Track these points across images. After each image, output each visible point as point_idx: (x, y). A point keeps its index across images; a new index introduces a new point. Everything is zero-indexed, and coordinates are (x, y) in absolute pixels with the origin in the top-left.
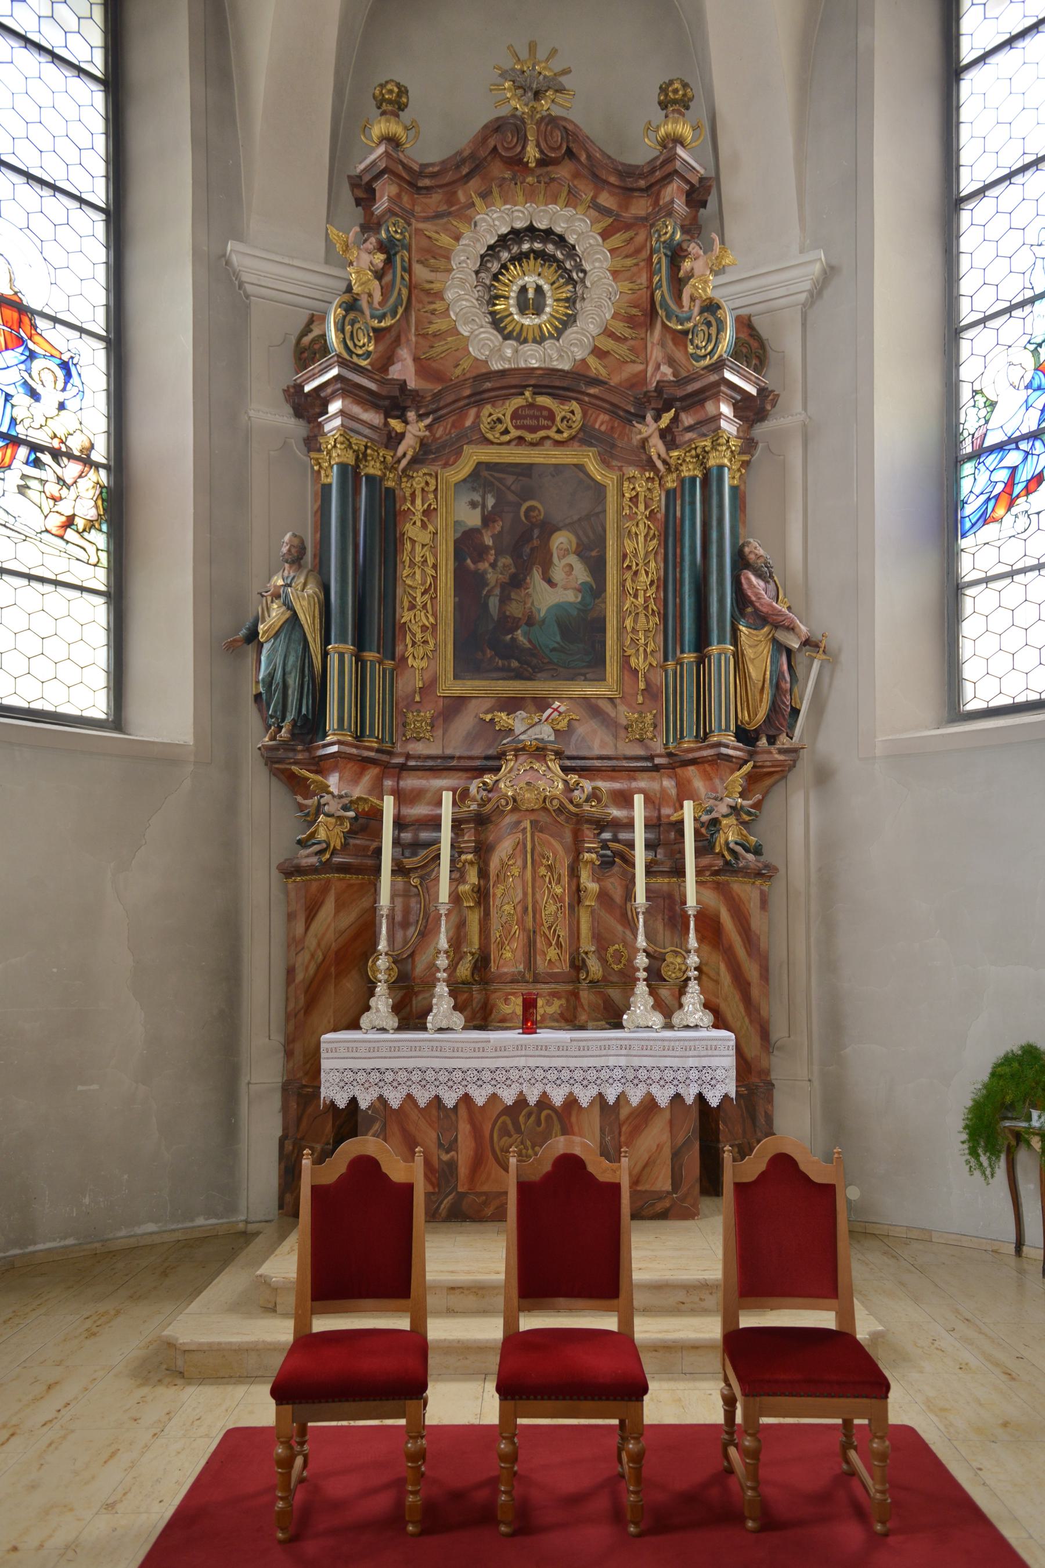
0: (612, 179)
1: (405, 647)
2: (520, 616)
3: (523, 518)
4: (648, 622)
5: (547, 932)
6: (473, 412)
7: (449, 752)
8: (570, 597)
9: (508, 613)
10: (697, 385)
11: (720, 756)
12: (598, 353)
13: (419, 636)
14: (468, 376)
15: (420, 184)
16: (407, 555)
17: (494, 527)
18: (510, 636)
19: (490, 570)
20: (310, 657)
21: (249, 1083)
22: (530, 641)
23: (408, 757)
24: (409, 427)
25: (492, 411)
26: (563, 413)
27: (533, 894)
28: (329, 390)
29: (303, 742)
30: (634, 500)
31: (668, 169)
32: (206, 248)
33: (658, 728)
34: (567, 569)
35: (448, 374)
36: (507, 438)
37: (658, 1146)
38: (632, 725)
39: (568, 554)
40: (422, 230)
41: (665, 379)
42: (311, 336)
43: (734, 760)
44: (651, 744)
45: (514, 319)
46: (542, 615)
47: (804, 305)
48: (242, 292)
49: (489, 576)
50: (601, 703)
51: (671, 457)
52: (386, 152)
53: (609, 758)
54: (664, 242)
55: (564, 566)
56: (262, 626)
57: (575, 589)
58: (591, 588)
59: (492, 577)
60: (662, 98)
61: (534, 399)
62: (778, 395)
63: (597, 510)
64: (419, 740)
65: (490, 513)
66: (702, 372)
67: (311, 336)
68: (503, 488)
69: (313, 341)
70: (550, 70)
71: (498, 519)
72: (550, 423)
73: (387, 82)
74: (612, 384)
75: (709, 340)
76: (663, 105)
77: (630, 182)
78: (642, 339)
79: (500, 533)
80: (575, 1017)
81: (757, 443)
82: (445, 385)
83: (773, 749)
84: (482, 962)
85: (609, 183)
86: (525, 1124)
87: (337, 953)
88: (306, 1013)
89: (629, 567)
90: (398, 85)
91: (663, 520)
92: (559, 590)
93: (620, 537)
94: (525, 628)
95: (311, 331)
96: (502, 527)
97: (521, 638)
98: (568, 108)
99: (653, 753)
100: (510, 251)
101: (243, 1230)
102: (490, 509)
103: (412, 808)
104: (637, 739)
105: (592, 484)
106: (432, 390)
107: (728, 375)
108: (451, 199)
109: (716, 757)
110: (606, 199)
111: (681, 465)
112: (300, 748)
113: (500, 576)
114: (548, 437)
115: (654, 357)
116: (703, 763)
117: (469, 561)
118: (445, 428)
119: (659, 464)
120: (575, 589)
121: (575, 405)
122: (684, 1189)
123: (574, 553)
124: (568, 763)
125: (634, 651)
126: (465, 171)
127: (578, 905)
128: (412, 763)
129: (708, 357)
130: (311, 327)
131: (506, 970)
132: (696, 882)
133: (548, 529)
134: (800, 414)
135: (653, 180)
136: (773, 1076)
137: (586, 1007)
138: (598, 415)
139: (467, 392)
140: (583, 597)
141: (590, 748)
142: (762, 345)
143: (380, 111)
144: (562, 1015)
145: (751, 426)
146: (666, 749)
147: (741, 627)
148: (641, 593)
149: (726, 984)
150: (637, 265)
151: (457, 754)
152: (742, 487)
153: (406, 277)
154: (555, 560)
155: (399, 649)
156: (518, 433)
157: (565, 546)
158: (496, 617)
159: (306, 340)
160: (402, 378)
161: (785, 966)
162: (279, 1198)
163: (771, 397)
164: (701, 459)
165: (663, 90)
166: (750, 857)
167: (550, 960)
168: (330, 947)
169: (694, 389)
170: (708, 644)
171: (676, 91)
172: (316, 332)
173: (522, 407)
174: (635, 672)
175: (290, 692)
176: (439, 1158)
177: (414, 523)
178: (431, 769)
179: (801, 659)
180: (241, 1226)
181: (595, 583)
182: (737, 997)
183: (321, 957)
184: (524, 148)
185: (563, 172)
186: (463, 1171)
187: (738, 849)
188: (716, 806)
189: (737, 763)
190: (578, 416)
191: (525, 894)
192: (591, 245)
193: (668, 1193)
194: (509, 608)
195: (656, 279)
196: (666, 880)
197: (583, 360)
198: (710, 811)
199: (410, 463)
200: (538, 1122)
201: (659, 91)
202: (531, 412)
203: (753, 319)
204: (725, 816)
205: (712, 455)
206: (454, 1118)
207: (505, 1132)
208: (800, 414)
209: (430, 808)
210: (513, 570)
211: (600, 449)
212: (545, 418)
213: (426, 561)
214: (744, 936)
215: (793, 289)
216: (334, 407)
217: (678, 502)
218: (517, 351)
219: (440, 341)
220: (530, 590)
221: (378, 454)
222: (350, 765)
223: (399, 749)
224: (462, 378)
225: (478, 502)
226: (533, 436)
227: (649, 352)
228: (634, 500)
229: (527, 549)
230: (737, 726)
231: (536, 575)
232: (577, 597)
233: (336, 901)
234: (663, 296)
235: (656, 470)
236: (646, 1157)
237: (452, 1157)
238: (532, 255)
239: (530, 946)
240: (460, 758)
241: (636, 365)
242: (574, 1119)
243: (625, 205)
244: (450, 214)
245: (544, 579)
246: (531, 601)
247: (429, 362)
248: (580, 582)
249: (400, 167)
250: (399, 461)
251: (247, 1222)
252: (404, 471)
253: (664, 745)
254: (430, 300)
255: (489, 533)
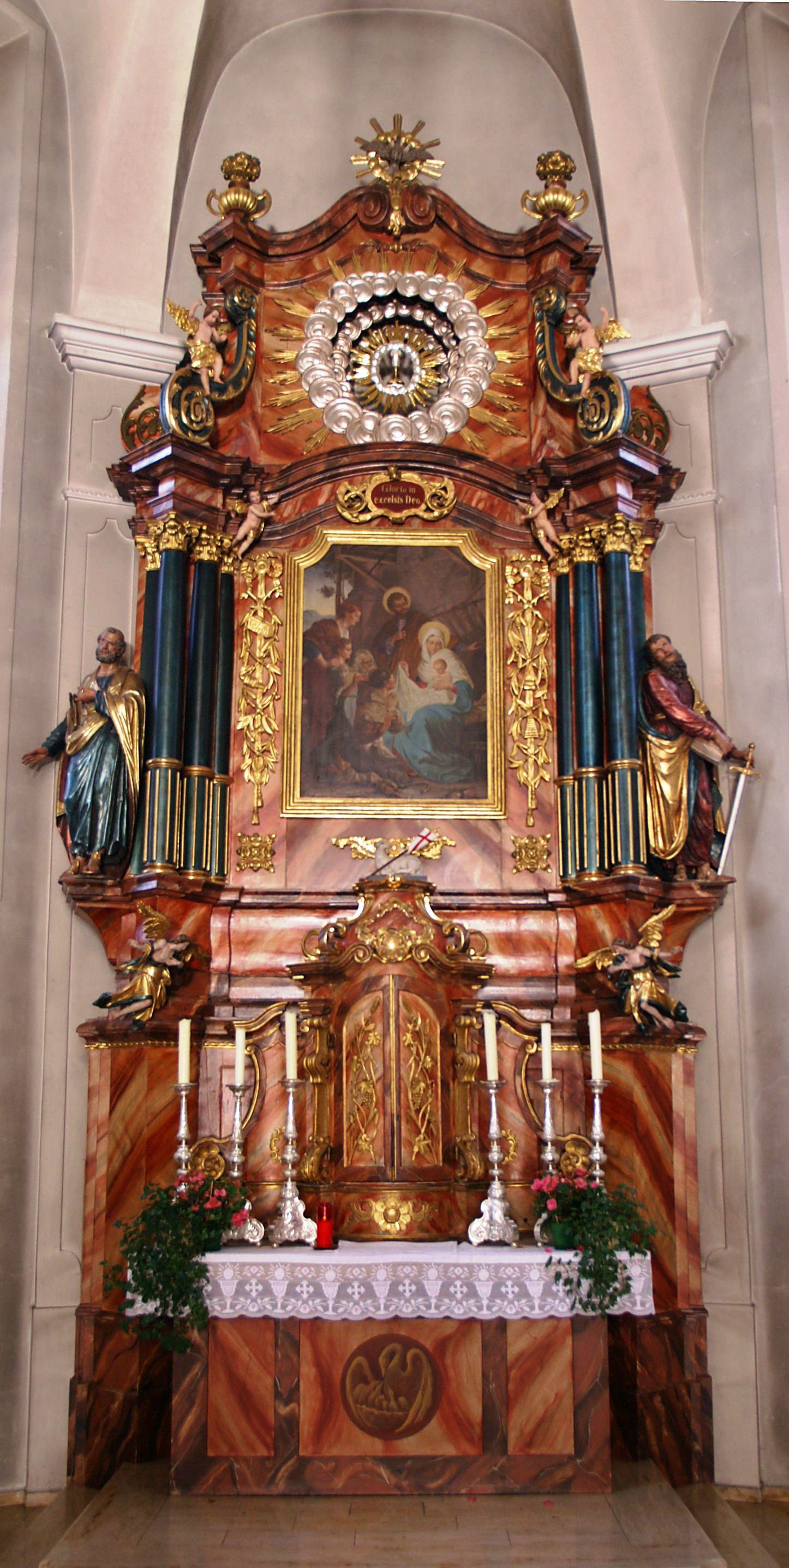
0: (487, 247)
1: (241, 760)
2: (382, 721)
3: (386, 607)
4: (539, 729)
5: (413, 1114)
6: (327, 489)
7: (293, 886)
8: (443, 698)
9: (367, 718)
10: (589, 464)
11: (628, 893)
12: (475, 425)
13: (258, 746)
14: (322, 450)
15: (271, 253)
16: (246, 650)
17: (351, 618)
18: (369, 745)
19: (346, 667)
20: (126, 772)
21: (34, 1307)
22: (394, 751)
23: (242, 892)
24: (252, 508)
25: (349, 487)
26: (434, 490)
27: (398, 1069)
28: (160, 470)
29: (114, 876)
30: (519, 586)
31: (550, 238)
32: (27, 321)
33: (553, 856)
34: (439, 666)
35: (300, 449)
36: (368, 517)
37: (557, 1395)
38: (520, 851)
39: (441, 648)
40: (272, 299)
41: (552, 455)
42: (141, 409)
43: (646, 898)
44: (545, 875)
45: (376, 389)
46: (409, 719)
47: (710, 376)
48: (65, 364)
49: (345, 674)
50: (481, 825)
51: (561, 540)
52: (234, 223)
53: (492, 894)
54: (548, 311)
55: (436, 663)
56: (69, 737)
57: (448, 689)
58: (468, 687)
59: (348, 675)
60: (542, 168)
61: (399, 475)
62: (684, 474)
63: (474, 598)
64: (256, 871)
65: (345, 601)
66: (594, 450)
67: (141, 409)
68: (363, 574)
69: (144, 414)
70: (418, 142)
71: (355, 607)
72: (418, 501)
73: (237, 155)
74: (491, 460)
75: (602, 416)
76: (542, 176)
77: (506, 250)
78: (525, 411)
79: (359, 623)
80: (451, 1226)
81: (662, 525)
82: (294, 461)
83: (693, 884)
84: (334, 1153)
85: (483, 251)
86: (387, 1366)
87: (149, 1141)
88: (107, 1218)
89: (514, 663)
90: (249, 158)
91: (554, 609)
92: (429, 690)
93: (501, 630)
94: (388, 735)
95: (142, 403)
96: (361, 618)
97: (383, 747)
98: (436, 178)
99: (547, 888)
100: (371, 317)
101: (21, 1501)
102: (346, 596)
103: (246, 956)
104: (527, 869)
105: (468, 567)
106: (279, 466)
107: (624, 454)
108: (305, 267)
109: (622, 895)
110: (479, 267)
111: (573, 549)
112: (110, 882)
113: (358, 674)
114: (416, 516)
115: (538, 431)
116: (608, 901)
117: (320, 657)
118: (295, 507)
119: (548, 547)
120: (448, 689)
121: (448, 482)
122: (590, 1452)
123: (448, 647)
124: (441, 900)
125: (521, 762)
126: (322, 239)
127: (454, 1081)
128: (246, 900)
129: (601, 434)
130: (142, 399)
131: (362, 1165)
132: (603, 1051)
133: (416, 619)
134: (711, 493)
135: (533, 249)
136: (707, 1300)
137: (464, 1213)
138: (476, 491)
139: (321, 468)
140: (458, 699)
141: (469, 881)
142: (665, 419)
143: (228, 182)
144: (433, 1223)
145: (655, 506)
146: (563, 882)
147: (650, 737)
148: (529, 694)
149: (642, 1183)
150: (517, 333)
151: (304, 889)
152: (646, 574)
153: (254, 346)
154: (425, 654)
155: (234, 761)
156: (380, 512)
157: (435, 639)
158: (352, 723)
159: (136, 413)
160: (246, 456)
161: (719, 1156)
162: (69, 1465)
163: (676, 476)
164: (598, 545)
165: (542, 161)
166: (668, 1022)
167: (418, 1153)
168: (140, 1134)
169: (587, 467)
170: (612, 757)
171: (556, 163)
172: (148, 404)
173: (386, 483)
174: (524, 787)
175: (101, 814)
176: (275, 1411)
177: (255, 614)
178: (271, 907)
179: (724, 773)
180: (19, 1498)
181: (474, 682)
182: (658, 1198)
183: (128, 1147)
184: (388, 217)
185: (433, 238)
186: (306, 1428)
187: (653, 1011)
188: (626, 955)
189: (649, 902)
190: (450, 495)
191: (386, 1068)
192: (464, 313)
193: (570, 1458)
194: (368, 711)
195: (539, 349)
196: (565, 1048)
197: (456, 433)
198: (617, 961)
199: (251, 547)
200: (403, 1365)
201: (537, 162)
202: (396, 490)
203: (652, 389)
204: (638, 969)
205: (610, 538)
206: (295, 1359)
207: (360, 1378)
208: (711, 493)
209: (269, 956)
210: (374, 667)
211: (477, 529)
212: (412, 495)
213: (268, 656)
214: (665, 1119)
215: (696, 360)
216: (166, 487)
217: (571, 590)
218: (378, 424)
219: (290, 414)
220: (394, 691)
221: (215, 537)
222: (171, 904)
223: (231, 882)
224: (315, 453)
225: (332, 589)
226: (397, 515)
227: (533, 426)
228: (519, 586)
229: (391, 643)
230: (649, 855)
231: (402, 671)
232: (451, 699)
233: (149, 1076)
234: (547, 365)
235: (545, 555)
236: (540, 1410)
237: (293, 1411)
238: (397, 322)
239: (392, 1134)
240: (306, 893)
241: (517, 439)
242: (448, 1361)
243: (502, 273)
244: (304, 281)
245: (411, 677)
246: (395, 704)
247: (276, 435)
248: (454, 680)
249: (249, 237)
250: (239, 543)
251: (26, 1492)
252: (243, 555)
253: (561, 877)
254: (280, 370)
255: (345, 625)
